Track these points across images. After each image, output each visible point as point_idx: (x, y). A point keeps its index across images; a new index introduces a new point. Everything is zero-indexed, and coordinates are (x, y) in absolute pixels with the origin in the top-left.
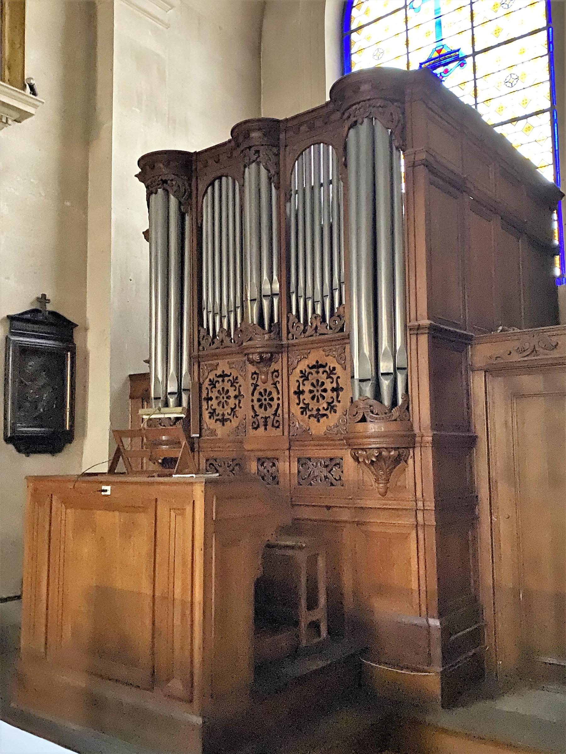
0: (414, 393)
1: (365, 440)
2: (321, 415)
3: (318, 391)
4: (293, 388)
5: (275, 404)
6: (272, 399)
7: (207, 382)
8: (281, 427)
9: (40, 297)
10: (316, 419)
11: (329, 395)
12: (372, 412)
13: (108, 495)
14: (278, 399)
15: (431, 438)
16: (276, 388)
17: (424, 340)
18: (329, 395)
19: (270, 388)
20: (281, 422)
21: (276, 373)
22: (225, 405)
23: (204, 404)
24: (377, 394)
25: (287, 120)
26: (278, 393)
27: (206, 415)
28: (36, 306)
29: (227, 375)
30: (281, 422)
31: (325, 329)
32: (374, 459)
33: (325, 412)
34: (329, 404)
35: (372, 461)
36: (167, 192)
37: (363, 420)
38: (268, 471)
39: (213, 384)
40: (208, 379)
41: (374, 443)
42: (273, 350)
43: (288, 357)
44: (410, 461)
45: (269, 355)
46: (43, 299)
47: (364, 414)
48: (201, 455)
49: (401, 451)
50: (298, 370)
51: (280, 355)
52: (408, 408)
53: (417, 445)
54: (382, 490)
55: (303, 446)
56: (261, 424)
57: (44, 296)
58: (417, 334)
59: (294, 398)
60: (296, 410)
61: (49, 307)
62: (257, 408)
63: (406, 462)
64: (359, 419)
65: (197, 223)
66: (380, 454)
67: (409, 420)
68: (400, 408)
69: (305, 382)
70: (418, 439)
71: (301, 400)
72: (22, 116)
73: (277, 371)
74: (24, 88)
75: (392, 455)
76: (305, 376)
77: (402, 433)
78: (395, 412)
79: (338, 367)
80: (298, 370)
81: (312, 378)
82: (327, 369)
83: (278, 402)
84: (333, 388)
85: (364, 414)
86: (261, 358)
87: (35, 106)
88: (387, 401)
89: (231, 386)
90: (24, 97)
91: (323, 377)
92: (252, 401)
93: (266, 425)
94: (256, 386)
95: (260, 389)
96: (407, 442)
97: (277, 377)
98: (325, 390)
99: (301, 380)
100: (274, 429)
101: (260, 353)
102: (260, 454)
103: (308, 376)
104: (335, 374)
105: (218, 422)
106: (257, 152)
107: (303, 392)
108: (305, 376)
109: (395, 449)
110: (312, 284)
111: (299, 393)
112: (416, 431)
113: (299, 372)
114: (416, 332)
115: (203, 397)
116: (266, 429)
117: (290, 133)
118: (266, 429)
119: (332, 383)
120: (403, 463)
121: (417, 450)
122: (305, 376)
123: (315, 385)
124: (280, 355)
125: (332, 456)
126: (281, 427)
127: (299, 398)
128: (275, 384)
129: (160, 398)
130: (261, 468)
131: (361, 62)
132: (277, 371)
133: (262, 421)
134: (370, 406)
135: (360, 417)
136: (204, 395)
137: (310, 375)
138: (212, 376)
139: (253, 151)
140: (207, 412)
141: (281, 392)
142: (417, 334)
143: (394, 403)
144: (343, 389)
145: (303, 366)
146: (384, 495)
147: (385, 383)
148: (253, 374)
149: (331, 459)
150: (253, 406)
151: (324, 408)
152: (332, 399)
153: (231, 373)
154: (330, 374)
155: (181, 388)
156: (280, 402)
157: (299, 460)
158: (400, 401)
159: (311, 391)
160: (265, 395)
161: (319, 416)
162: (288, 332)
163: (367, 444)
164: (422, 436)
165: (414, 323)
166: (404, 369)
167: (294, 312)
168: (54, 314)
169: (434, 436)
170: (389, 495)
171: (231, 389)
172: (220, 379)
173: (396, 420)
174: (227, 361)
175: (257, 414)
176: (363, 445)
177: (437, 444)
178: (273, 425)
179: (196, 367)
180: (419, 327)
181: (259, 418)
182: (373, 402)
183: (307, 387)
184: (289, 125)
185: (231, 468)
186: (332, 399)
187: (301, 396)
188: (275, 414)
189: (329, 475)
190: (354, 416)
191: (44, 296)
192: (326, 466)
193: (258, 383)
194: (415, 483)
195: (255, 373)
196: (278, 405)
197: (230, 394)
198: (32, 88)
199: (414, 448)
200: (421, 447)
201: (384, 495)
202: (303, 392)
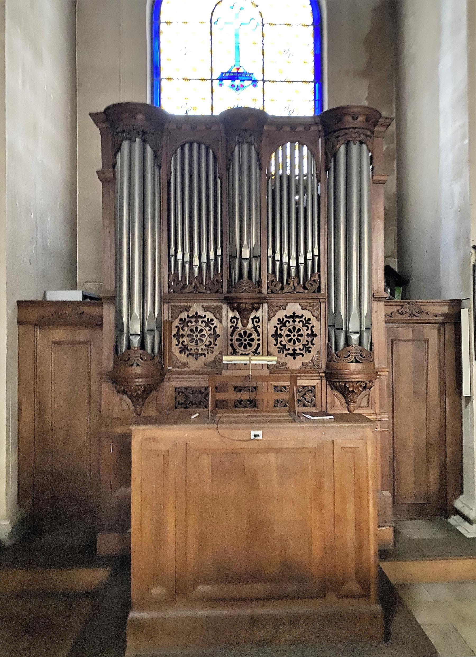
1: (347, 376)
4: (174, 332)
5: (255, 344)
6: (253, 340)
13: (261, 440)
18: (304, 340)
32: (139, 392)
36: (144, 141)
59: (174, 341)
69: (282, 328)
71: (279, 342)
76: (306, 323)
81: (290, 325)
83: (258, 342)
92: (231, 340)
104: (310, 324)
105: (288, 356)
111: (178, 336)
115: (173, 334)
129: (342, 329)
131: (214, 114)
132: (258, 318)
140: (177, 347)
144: (220, 336)
148: (232, 318)
152: (307, 343)
154: (306, 323)
159: (287, 335)
161: (294, 355)
174: (201, 304)
185: (188, 401)
186: (307, 343)
190: (345, 358)
193: (237, 326)
195: (235, 317)
197: (204, 332)
202: (281, 336)
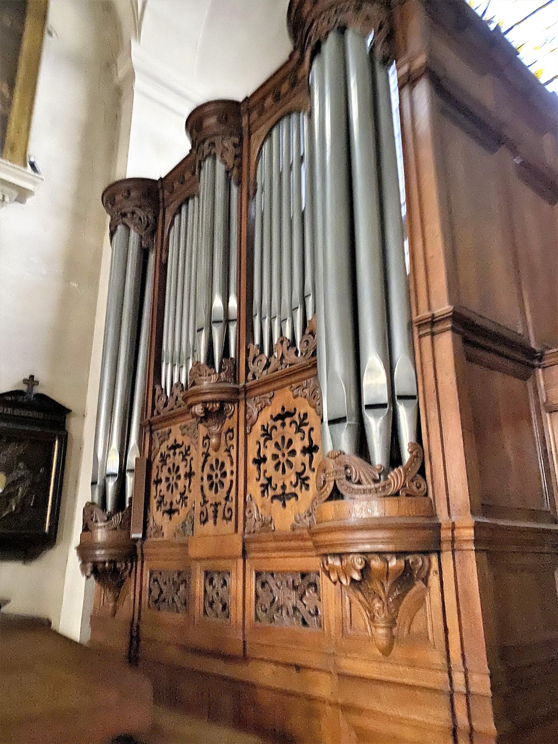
0: (433, 443)
2: (288, 495)
3: (283, 455)
4: (253, 454)
6: (224, 474)
7: (158, 457)
8: (233, 518)
9: (28, 378)
10: (281, 503)
11: (299, 458)
12: (349, 478)
14: (232, 472)
15: (472, 532)
16: (230, 456)
17: (446, 343)
19: (223, 456)
20: (234, 511)
21: (230, 434)
22: (174, 489)
23: (153, 488)
24: (362, 448)
25: (246, 99)
26: (232, 463)
27: (154, 503)
28: (24, 388)
29: (179, 446)
30: (234, 511)
31: (295, 357)
32: (357, 577)
33: (293, 490)
34: (299, 475)
35: (353, 580)
37: (336, 495)
38: (218, 594)
39: (164, 461)
40: (159, 454)
41: (365, 542)
42: (225, 396)
43: (246, 405)
44: (434, 580)
45: (218, 405)
46: (31, 381)
47: (335, 484)
48: (248, 566)
49: (411, 559)
50: (258, 428)
51: (236, 405)
52: (422, 471)
53: (444, 546)
54: (383, 641)
55: (263, 550)
56: (211, 514)
57: (32, 377)
58: (433, 334)
59: (252, 467)
60: (255, 488)
61: (38, 390)
62: (206, 488)
63: (425, 581)
64: (327, 497)
65: (161, 257)
66: (367, 565)
67: (426, 495)
68: (407, 469)
70: (445, 534)
72: (22, 195)
73: (232, 431)
74: (25, 166)
75: (393, 569)
77: (409, 521)
78: (396, 478)
79: (311, 412)
80: (258, 428)
82: (296, 417)
84: (304, 447)
85: (335, 484)
86: (206, 410)
87: (35, 183)
88: (378, 455)
89: (183, 460)
90: (25, 175)
91: (290, 431)
93: (215, 517)
94: (207, 455)
95: (211, 460)
96: (430, 540)
97: (231, 439)
98: (293, 453)
99: (262, 440)
100: (225, 521)
101: (205, 402)
102: (209, 565)
103: (271, 433)
106: (213, 144)
107: (264, 459)
108: (267, 435)
109: (398, 554)
110: (276, 292)
111: (260, 461)
112: (443, 517)
113: (260, 428)
114: (429, 330)
116: (215, 523)
117: (254, 115)
118: (215, 523)
119: (302, 439)
120: (419, 584)
121: (447, 557)
122: (267, 434)
123: (280, 443)
124: (236, 405)
125: (304, 569)
126: (233, 518)
127: (259, 468)
128: (228, 451)
130: (209, 588)
133: (211, 510)
134: (347, 467)
135: (329, 489)
136: (154, 477)
137: (274, 430)
138: (163, 449)
139: (207, 144)
141: (235, 461)
142: (433, 334)
143: (394, 458)
145: (265, 418)
146: (387, 651)
147: (375, 425)
149: (304, 575)
150: (202, 487)
151: (291, 483)
153: (183, 443)
154: (300, 426)
155: (125, 468)
156: (234, 477)
157: (258, 574)
158: (406, 456)
160: (217, 469)
162: (247, 370)
163: (341, 545)
164: (453, 528)
165: (425, 313)
166: (413, 397)
167: (257, 341)
168: (42, 397)
169: (477, 527)
170: (397, 651)
171: (182, 465)
172: (172, 452)
173: (397, 494)
174: (179, 425)
175: (206, 499)
176: (333, 545)
177: (488, 543)
178: (224, 517)
179: (148, 435)
180: (433, 321)
181: (208, 505)
182: (356, 461)
183: (269, 451)
184: (251, 104)
187: (262, 465)
188: (227, 498)
189: (300, 605)
191: (32, 377)
192: (295, 588)
194: (446, 630)
196: (232, 482)
198: (33, 165)
199: (439, 552)
200: (453, 551)
201: (387, 651)
